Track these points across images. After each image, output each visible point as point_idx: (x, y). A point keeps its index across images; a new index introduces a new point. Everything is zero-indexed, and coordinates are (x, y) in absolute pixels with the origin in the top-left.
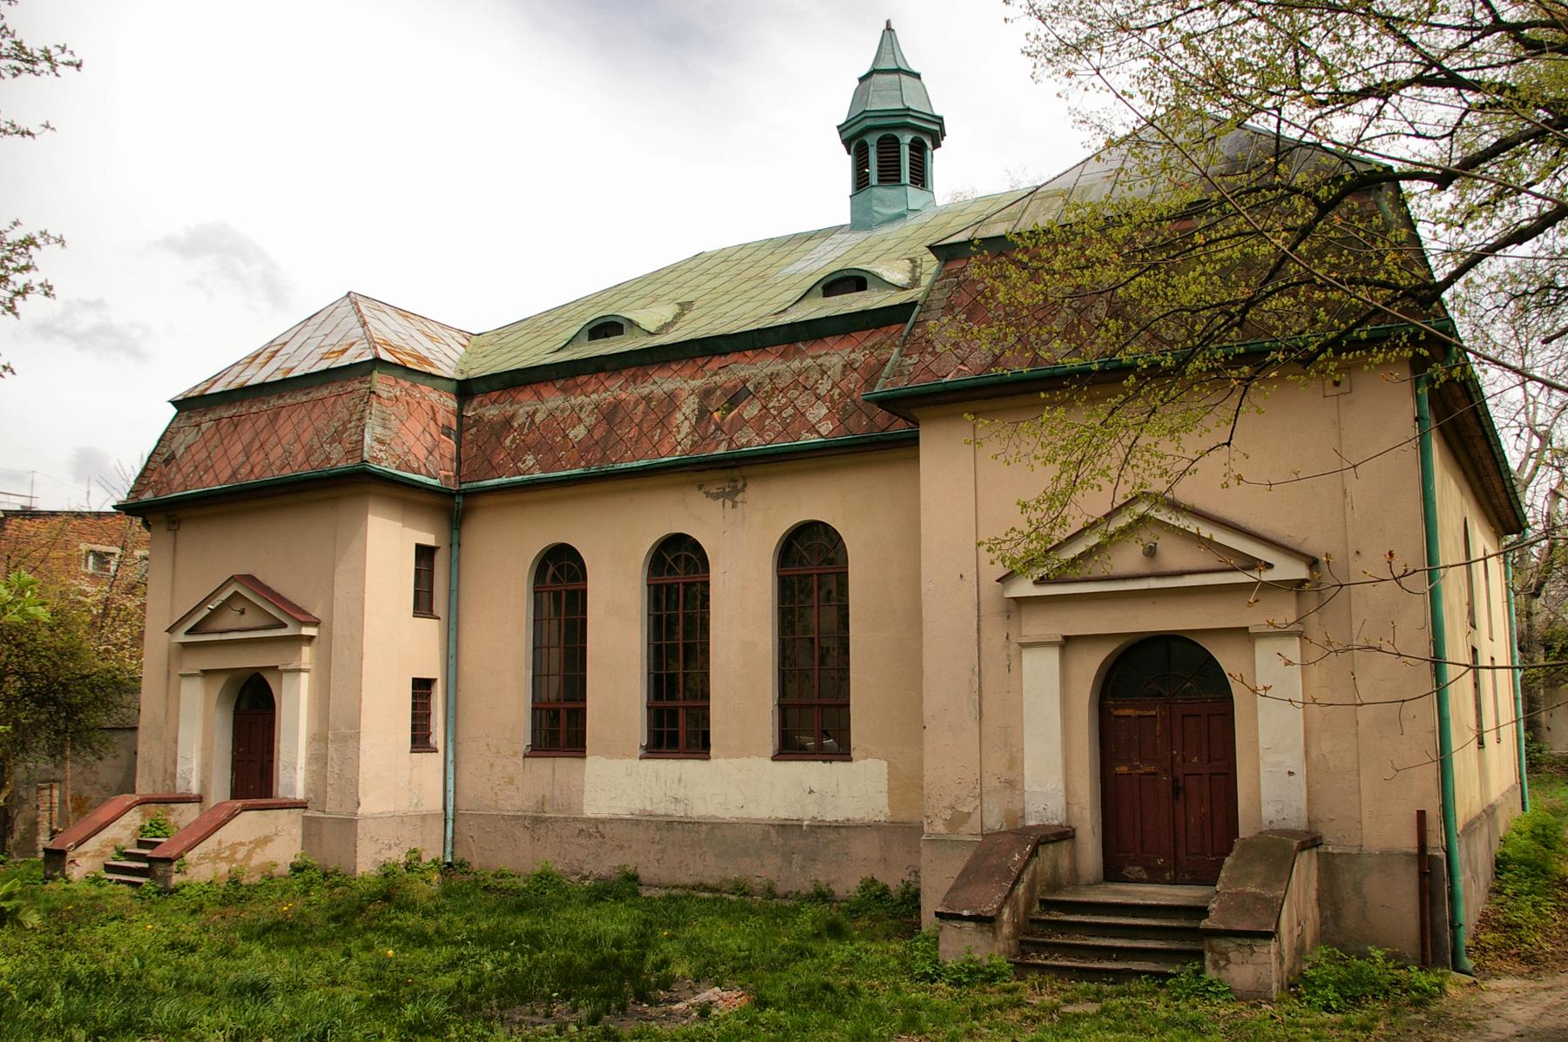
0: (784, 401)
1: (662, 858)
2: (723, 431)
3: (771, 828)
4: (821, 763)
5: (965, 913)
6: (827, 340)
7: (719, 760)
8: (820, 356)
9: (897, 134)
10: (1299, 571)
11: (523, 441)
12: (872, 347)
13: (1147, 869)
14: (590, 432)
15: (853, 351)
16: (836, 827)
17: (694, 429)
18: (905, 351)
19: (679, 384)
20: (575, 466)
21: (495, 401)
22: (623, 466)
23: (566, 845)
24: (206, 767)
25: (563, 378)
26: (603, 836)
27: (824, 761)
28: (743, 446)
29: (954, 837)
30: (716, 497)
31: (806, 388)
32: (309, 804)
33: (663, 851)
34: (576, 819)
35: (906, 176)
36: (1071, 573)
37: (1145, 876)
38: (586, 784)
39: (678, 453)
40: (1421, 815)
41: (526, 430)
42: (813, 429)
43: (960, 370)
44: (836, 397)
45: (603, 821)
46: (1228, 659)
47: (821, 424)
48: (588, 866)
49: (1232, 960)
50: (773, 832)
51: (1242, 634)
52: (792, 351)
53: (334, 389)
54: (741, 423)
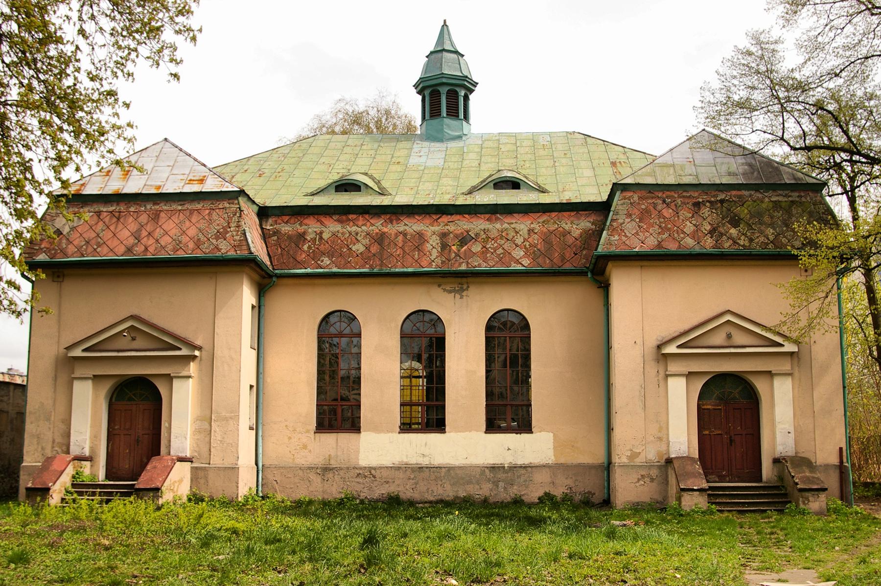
0: (496, 245)
1: (415, 487)
2: (461, 257)
3: (486, 469)
4: (515, 434)
5: (695, 488)
6: (514, 215)
7: (452, 434)
8: (513, 223)
9: (458, 89)
10: (794, 348)
11: (317, 248)
12: (543, 222)
13: (719, 476)
14: (368, 248)
15: (532, 223)
16: (525, 467)
17: (441, 254)
18: (610, 233)
19: (423, 227)
20: (363, 267)
21: (287, 221)
22: (397, 270)
23: (348, 483)
24: (95, 437)
25: (337, 214)
26: (374, 477)
27: (517, 433)
28: (476, 266)
29: (632, 464)
30: (450, 292)
31: (508, 240)
32: (193, 460)
33: (416, 484)
34: (354, 468)
35: (462, 116)
36: (689, 345)
37: (717, 480)
38: (361, 448)
39: (434, 267)
40: (841, 449)
41: (317, 243)
42: (518, 262)
43: (642, 246)
44: (528, 246)
45: (375, 469)
46: (760, 385)
47: (522, 261)
48: (364, 494)
49: (811, 500)
50: (487, 471)
51: (770, 374)
52: (494, 219)
53: (207, 204)
54: (470, 254)
